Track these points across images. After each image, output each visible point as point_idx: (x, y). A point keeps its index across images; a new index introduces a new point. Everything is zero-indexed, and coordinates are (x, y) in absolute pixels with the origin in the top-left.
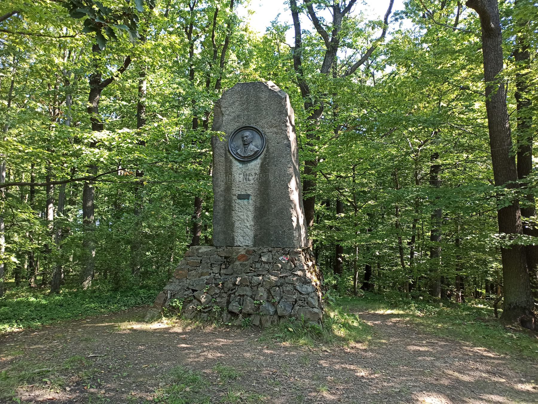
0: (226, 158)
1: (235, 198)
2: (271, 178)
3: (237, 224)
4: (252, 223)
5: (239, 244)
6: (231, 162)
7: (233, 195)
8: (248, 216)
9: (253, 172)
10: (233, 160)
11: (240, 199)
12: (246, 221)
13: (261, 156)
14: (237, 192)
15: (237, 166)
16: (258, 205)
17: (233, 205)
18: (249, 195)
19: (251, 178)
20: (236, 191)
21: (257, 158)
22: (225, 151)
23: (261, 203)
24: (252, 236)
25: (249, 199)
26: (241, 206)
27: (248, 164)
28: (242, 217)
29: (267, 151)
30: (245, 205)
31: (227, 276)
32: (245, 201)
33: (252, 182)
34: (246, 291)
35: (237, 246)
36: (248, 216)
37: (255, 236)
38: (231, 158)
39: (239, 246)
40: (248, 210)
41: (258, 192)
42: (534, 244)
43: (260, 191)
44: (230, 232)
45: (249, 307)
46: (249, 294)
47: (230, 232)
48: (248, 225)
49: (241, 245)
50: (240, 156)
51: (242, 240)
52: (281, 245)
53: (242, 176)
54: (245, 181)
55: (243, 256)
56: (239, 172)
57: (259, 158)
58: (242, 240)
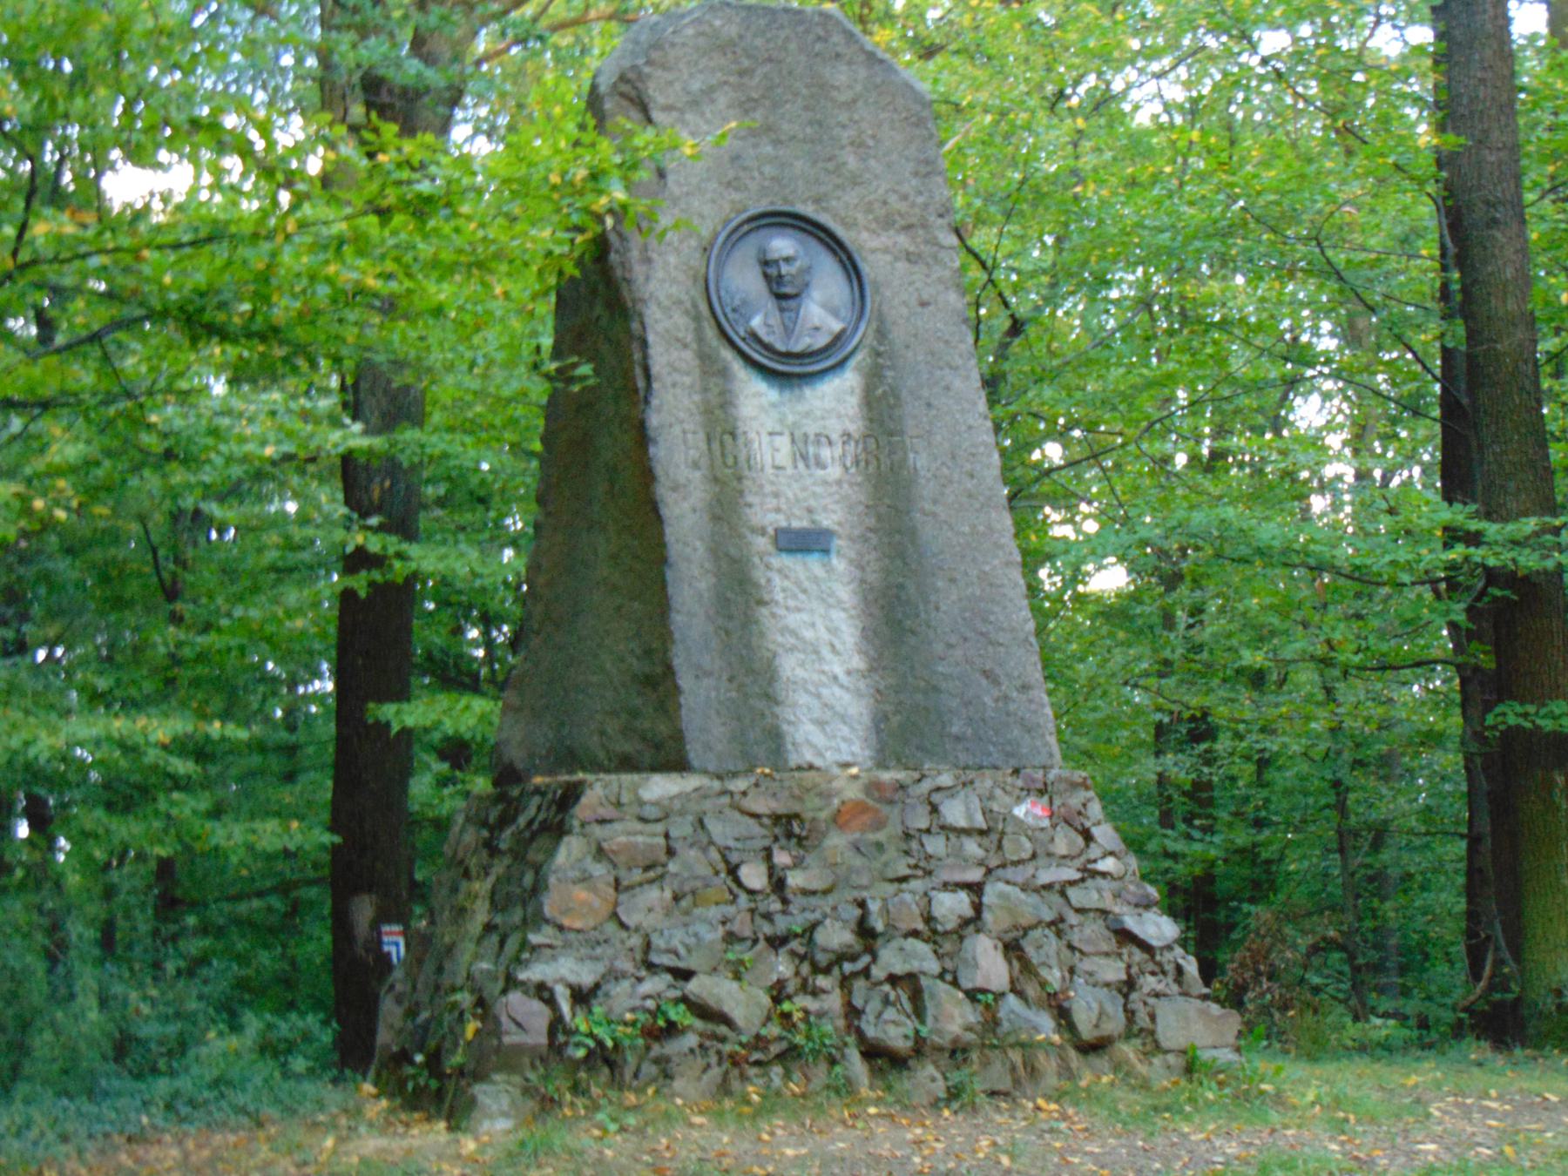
0: (706, 359)
1: (762, 543)
2: (920, 460)
3: (790, 667)
4: (858, 662)
5: (809, 756)
6: (725, 373)
7: (753, 530)
8: (834, 631)
9: (835, 428)
10: (738, 368)
11: (789, 551)
12: (826, 652)
13: (859, 357)
14: (771, 517)
15: (756, 398)
16: (872, 578)
17: (759, 575)
18: (827, 534)
19: (826, 453)
20: (766, 513)
21: (841, 364)
22: (697, 318)
23: (887, 572)
24: (866, 719)
25: (826, 551)
26: (798, 583)
27: (807, 392)
28: (808, 634)
29: (881, 334)
30: (815, 580)
31: (813, 901)
32: (814, 562)
33: (834, 472)
34: (915, 955)
35: (799, 768)
36: (834, 631)
37: (879, 721)
38: (727, 354)
39: (811, 767)
40: (827, 599)
41: (871, 522)
42: (1240, 280)
43: (879, 518)
44: (760, 704)
45: (954, 1017)
46: (933, 966)
47: (760, 704)
48: (838, 670)
49: (818, 762)
50: (768, 347)
51: (819, 739)
52: (996, 757)
53: (784, 443)
54: (801, 465)
55: (860, 808)
56: (770, 423)
57: (852, 363)
58: (819, 739)
